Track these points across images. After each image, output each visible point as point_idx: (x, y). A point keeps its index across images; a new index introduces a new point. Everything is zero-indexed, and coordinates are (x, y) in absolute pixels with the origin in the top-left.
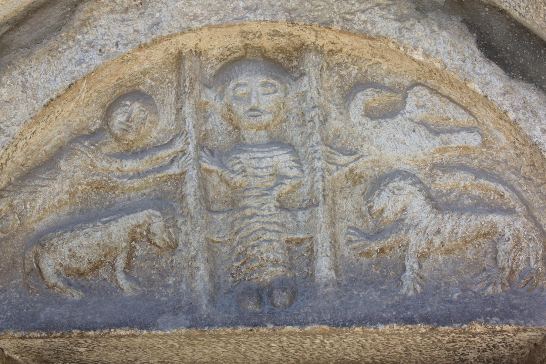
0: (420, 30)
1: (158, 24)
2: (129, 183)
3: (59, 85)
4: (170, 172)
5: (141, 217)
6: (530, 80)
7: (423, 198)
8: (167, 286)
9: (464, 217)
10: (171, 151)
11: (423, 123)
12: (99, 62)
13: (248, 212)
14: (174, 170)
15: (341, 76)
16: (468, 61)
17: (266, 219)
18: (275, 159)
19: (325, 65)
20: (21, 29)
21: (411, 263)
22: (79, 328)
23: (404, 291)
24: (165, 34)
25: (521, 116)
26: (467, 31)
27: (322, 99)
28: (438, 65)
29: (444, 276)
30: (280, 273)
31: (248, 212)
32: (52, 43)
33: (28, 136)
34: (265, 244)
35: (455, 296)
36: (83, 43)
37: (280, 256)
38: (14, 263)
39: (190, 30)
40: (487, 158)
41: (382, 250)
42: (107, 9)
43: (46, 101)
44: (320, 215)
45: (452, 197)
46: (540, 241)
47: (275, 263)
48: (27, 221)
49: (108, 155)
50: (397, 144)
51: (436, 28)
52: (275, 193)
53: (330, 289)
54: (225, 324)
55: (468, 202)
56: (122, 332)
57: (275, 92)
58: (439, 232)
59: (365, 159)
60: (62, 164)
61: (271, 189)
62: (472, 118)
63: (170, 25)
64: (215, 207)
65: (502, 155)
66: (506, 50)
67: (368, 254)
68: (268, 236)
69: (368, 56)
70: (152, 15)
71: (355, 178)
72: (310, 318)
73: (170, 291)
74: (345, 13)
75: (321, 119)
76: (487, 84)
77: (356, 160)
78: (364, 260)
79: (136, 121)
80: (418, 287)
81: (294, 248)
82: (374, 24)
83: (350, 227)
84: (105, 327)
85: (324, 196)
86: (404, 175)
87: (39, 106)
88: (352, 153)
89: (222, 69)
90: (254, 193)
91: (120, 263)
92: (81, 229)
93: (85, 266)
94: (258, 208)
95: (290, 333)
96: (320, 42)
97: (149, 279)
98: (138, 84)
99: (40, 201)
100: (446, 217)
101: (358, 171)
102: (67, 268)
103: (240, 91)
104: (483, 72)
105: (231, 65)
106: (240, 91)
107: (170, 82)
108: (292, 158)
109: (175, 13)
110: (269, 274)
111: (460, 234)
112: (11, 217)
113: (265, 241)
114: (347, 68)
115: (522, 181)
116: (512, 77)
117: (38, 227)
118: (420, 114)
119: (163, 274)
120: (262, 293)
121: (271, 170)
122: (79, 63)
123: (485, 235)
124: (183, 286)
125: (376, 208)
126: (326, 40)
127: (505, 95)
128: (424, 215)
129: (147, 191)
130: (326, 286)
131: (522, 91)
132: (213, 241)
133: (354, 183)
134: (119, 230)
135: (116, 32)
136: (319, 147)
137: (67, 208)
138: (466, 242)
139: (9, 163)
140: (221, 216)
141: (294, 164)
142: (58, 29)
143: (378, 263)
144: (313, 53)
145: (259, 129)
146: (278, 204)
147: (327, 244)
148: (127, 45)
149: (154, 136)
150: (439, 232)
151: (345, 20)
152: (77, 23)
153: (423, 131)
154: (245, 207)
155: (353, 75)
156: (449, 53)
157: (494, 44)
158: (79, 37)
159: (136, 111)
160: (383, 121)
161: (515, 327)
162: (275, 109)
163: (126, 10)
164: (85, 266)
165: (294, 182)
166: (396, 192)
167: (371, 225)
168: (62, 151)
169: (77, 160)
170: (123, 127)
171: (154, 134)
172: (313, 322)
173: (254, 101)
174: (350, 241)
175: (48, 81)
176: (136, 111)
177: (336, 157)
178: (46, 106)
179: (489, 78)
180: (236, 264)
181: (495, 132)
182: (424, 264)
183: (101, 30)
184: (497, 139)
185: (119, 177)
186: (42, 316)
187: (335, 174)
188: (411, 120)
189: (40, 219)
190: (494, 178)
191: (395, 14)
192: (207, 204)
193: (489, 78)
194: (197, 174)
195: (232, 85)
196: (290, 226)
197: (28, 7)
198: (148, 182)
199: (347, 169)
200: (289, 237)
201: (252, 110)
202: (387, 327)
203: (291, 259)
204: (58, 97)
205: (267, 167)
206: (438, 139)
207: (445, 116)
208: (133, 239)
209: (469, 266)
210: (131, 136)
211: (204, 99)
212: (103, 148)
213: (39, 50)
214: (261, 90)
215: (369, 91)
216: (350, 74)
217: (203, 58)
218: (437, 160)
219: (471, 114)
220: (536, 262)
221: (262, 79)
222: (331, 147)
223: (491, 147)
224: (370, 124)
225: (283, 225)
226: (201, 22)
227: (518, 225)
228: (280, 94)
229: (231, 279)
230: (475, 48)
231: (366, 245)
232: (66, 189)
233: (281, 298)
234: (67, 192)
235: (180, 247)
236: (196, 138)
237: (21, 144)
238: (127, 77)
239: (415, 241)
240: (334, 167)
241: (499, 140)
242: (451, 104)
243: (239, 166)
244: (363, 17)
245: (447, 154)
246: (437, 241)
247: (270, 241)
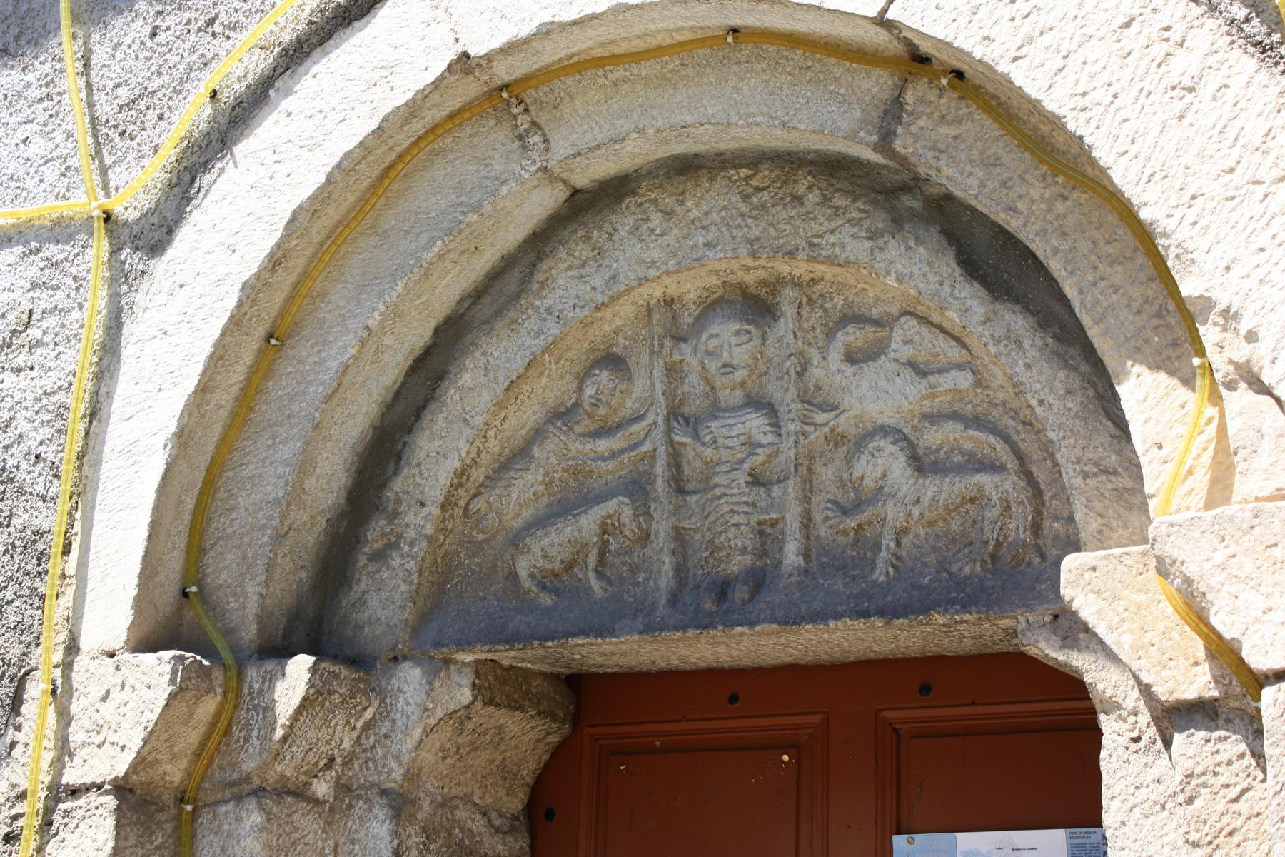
0: (894, 248)
1: (614, 277)
2: (603, 466)
3: (520, 363)
4: (644, 449)
5: (611, 505)
6: (1016, 301)
7: (904, 459)
8: (637, 584)
9: (947, 480)
10: (644, 423)
11: (911, 364)
12: (557, 332)
13: (717, 492)
14: (647, 447)
15: (826, 310)
16: (946, 283)
17: (735, 499)
18: (748, 424)
19: (805, 299)
20: (483, 301)
21: (888, 541)
22: (539, 639)
23: (874, 576)
24: (622, 288)
25: (1002, 349)
26: (946, 244)
27: (800, 343)
28: (913, 292)
29: (922, 555)
30: (749, 562)
31: (717, 492)
32: (512, 314)
33: (498, 423)
34: (733, 529)
35: (926, 580)
36: (542, 310)
37: (748, 542)
38: (496, 566)
39: (647, 280)
40: (983, 401)
41: (860, 526)
42: (565, 265)
43: (507, 383)
44: (790, 490)
45: (942, 454)
46: (1031, 504)
47: (744, 551)
48: (505, 519)
49: (582, 435)
50: (879, 395)
51: (912, 244)
52: (746, 466)
53: (793, 579)
54: (676, 628)
55: (958, 459)
56: (580, 641)
57: (750, 340)
58: (918, 501)
59: (847, 414)
60: (536, 451)
61: (742, 462)
62: (964, 352)
63: (627, 277)
64: (690, 487)
65: (1001, 395)
66: (988, 264)
67: (845, 533)
68: (736, 519)
69: (853, 282)
70: (609, 266)
71: (836, 439)
72: (762, 617)
73: (639, 590)
74: (814, 236)
75: (799, 369)
76: (967, 310)
77: (837, 416)
78: (841, 539)
79: (606, 392)
80: (891, 571)
81: (768, 530)
82: (843, 246)
83: (829, 501)
84: (563, 637)
85: (796, 466)
86: (884, 431)
87: (500, 390)
88: (834, 408)
89: (701, 314)
90: (725, 468)
91: (592, 560)
92: (553, 524)
93: (558, 566)
94: (726, 487)
95: (741, 635)
96: (796, 273)
97: (620, 576)
98: (612, 346)
99: (515, 496)
100: (928, 482)
101: (840, 430)
102: (541, 570)
103: (713, 343)
104: (963, 295)
105: (711, 307)
106: (713, 343)
107: (644, 339)
108: (767, 421)
109: (633, 261)
110: (738, 564)
111: (941, 502)
112: (490, 516)
113: (733, 525)
114: (832, 299)
115: (1020, 428)
116: (996, 298)
117: (517, 524)
118: (906, 353)
119: (634, 569)
120: (722, 589)
121: (742, 438)
122: (539, 334)
123: (972, 500)
124: (652, 583)
125: (856, 475)
126: (801, 269)
127: (985, 323)
128: (904, 481)
129: (623, 473)
130: (790, 575)
131: (1007, 316)
132: (684, 529)
133: (836, 446)
134: (588, 523)
135: (573, 292)
136: (793, 406)
137: (545, 500)
138: (949, 512)
139: (483, 455)
140: (695, 498)
141: (768, 428)
142: (517, 296)
143: (856, 542)
144: (790, 286)
145: (734, 388)
146: (749, 479)
147: (796, 525)
148: (582, 307)
149: (630, 405)
150: (918, 501)
151: (811, 245)
152: (536, 287)
153: (909, 373)
154: (716, 486)
155: (839, 307)
156: (925, 275)
157: (975, 257)
158: (538, 303)
159: (604, 382)
160: (864, 365)
161: (976, 616)
162: (750, 362)
163: (584, 265)
164: (558, 566)
165: (768, 451)
166: (876, 454)
167: (852, 495)
168: (538, 434)
169: (552, 444)
170: (593, 401)
171: (629, 404)
172: (764, 621)
173: (726, 355)
174: (827, 518)
175: (508, 360)
176: (604, 382)
177: (814, 415)
178: (507, 389)
179: (969, 302)
180: (705, 555)
181: (991, 366)
182: (904, 541)
183: (560, 292)
184: (993, 376)
185: (593, 460)
186: (511, 626)
187: (812, 437)
188: (896, 360)
189: (518, 516)
190: (986, 427)
191: (868, 230)
192: (679, 486)
193: (969, 302)
194: (666, 450)
195: (704, 337)
196: (763, 504)
197: (488, 273)
198: (622, 463)
199: (826, 429)
200: (761, 518)
201: (725, 366)
202: (839, 623)
203: (763, 544)
204: (519, 377)
205: (737, 436)
206: (924, 382)
207: (934, 351)
208: (605, 532)
209: (954, 540)
210: (602, 411)
211: (677, 357)
212: (576, 428)
213: (499, 325)
214: (734, 340)
215: (850, 329)
216: (835, 306)
217: (676, 306)
218: (927, 409)
219: (964, 346)
220: (1025, 531)
221: (735, 326)
222: (810, 403)
223: (987, 387)
224: (850, 370)
225: (754, 505)
226: (658, 268)
227: (1007, 486)
228: (757, 342)
229: (700, 572)
230: (955, 266)
231: (841, 522)
232: (540, 479)
233: (740, 593)
234: (543, 482)
235: (653, 537)
236: (667, 406)
237: (491, 433)
238: (599, 339)
239: (892, 513)
240: (812, 429)
241: (995, 377)
242: (941, 335)
243: (709, 437)
244: (832, 239)
245: (937, 400)
246: (916, 512)
247: (737, 525)
